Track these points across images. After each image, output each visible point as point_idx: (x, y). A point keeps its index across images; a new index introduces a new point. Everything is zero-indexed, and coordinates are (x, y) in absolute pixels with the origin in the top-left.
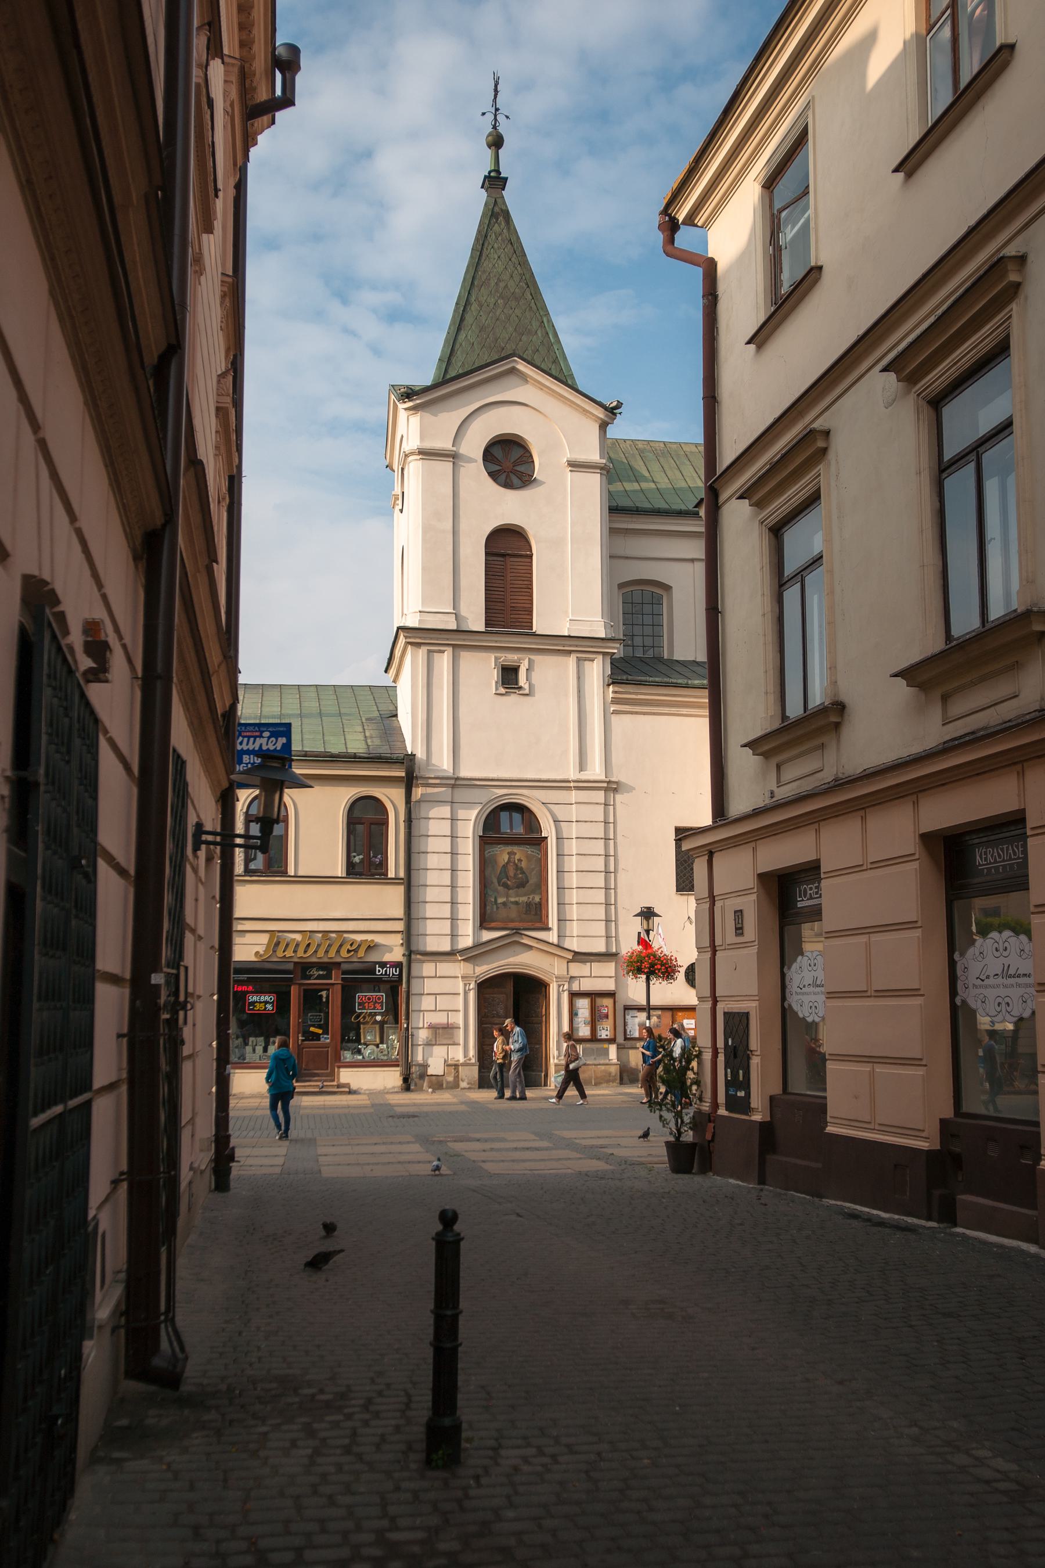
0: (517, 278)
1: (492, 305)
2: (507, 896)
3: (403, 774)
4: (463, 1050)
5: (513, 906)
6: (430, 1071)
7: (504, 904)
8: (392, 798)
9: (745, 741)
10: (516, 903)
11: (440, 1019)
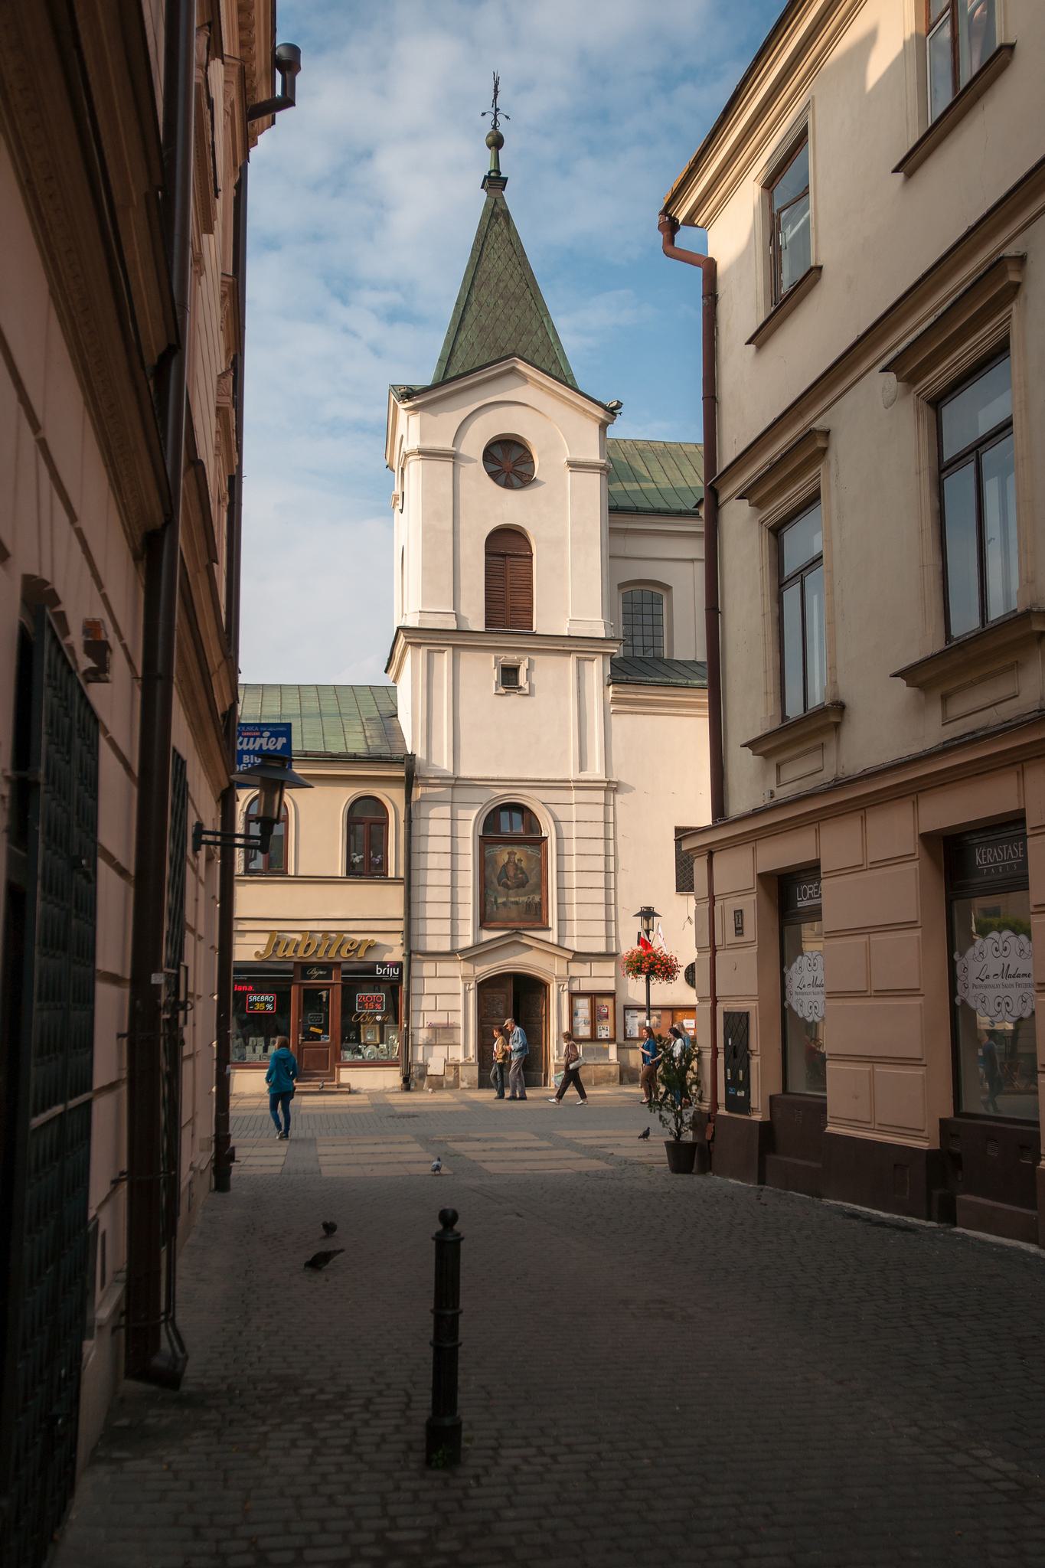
0: (517, 278)
2: (508, 896)
4: (463, 1050)
5: (513, 907)
6: (430, 1071)
7: (504, 904)
8: (392, 798)
9: (744, 742)
10: (517, 903)
11: (440, 1019)
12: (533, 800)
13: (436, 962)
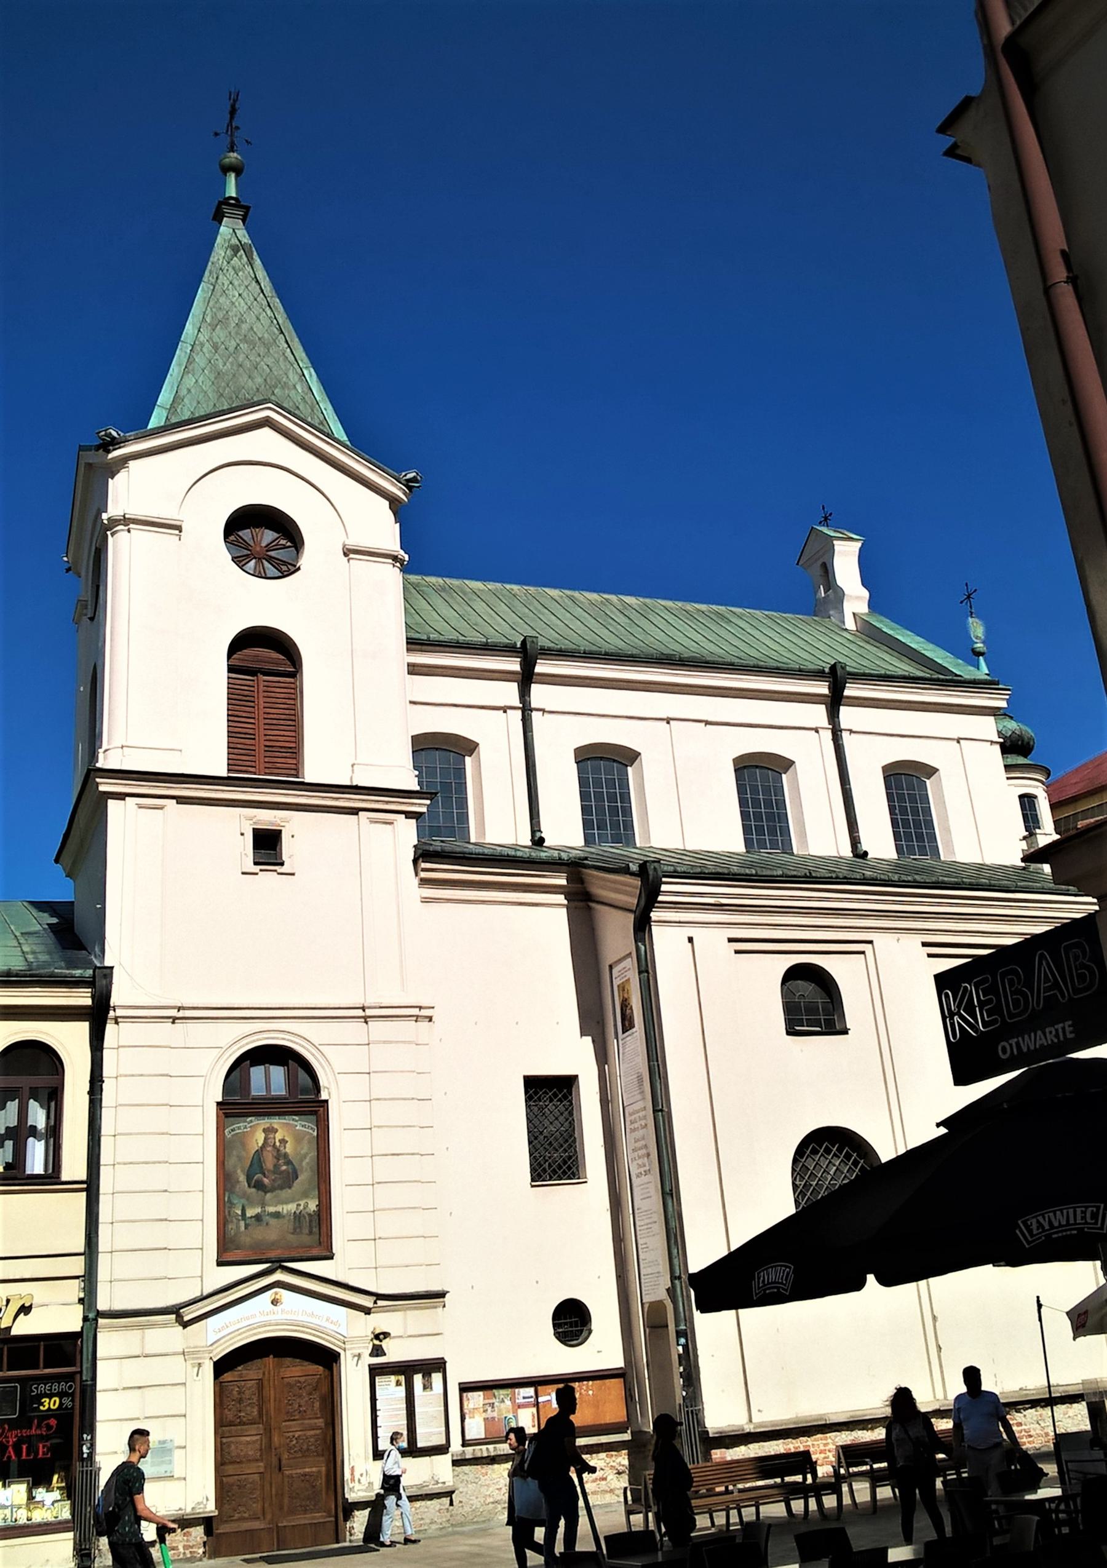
0: (265, 321)
1: (231, 349)
2: (263, 1205)
3: (88, 1002)
5: (273, 1222)
7: (258, 1218)
10: (277, 1215)
12: (830, 964)
13: (142, 1327)
